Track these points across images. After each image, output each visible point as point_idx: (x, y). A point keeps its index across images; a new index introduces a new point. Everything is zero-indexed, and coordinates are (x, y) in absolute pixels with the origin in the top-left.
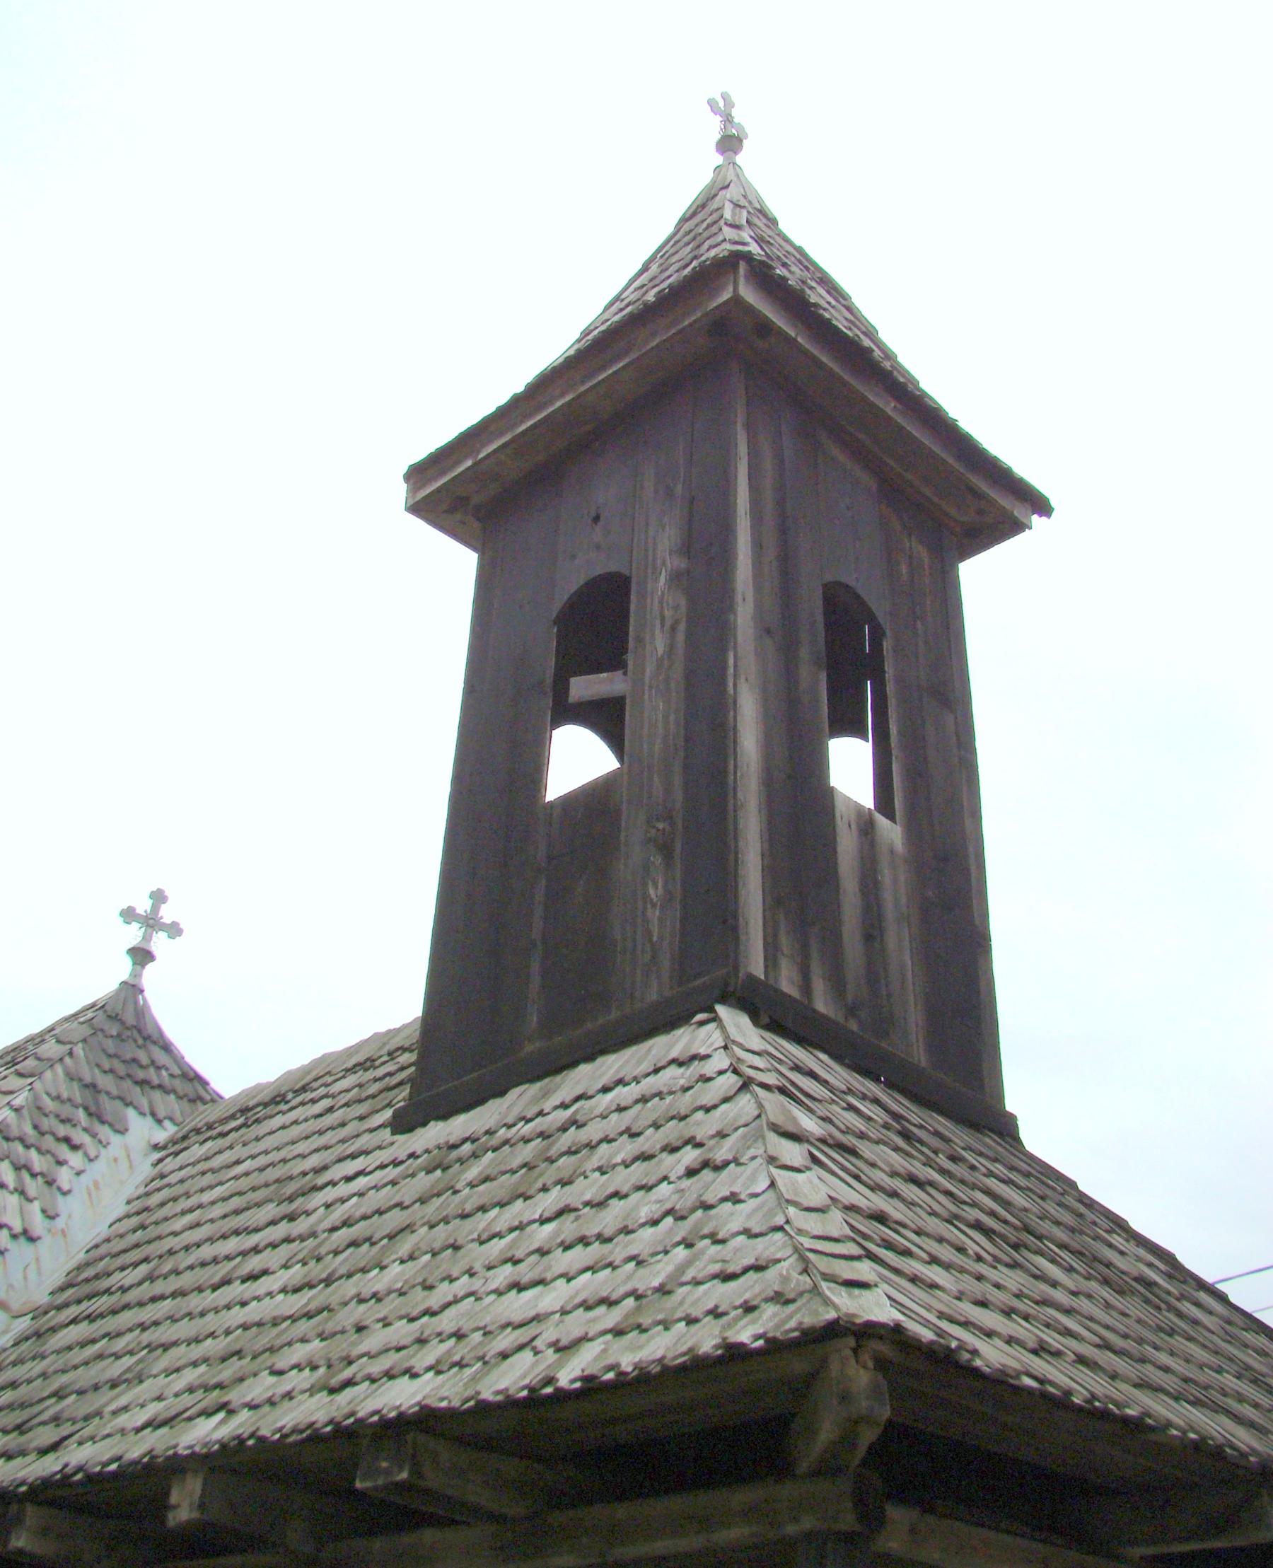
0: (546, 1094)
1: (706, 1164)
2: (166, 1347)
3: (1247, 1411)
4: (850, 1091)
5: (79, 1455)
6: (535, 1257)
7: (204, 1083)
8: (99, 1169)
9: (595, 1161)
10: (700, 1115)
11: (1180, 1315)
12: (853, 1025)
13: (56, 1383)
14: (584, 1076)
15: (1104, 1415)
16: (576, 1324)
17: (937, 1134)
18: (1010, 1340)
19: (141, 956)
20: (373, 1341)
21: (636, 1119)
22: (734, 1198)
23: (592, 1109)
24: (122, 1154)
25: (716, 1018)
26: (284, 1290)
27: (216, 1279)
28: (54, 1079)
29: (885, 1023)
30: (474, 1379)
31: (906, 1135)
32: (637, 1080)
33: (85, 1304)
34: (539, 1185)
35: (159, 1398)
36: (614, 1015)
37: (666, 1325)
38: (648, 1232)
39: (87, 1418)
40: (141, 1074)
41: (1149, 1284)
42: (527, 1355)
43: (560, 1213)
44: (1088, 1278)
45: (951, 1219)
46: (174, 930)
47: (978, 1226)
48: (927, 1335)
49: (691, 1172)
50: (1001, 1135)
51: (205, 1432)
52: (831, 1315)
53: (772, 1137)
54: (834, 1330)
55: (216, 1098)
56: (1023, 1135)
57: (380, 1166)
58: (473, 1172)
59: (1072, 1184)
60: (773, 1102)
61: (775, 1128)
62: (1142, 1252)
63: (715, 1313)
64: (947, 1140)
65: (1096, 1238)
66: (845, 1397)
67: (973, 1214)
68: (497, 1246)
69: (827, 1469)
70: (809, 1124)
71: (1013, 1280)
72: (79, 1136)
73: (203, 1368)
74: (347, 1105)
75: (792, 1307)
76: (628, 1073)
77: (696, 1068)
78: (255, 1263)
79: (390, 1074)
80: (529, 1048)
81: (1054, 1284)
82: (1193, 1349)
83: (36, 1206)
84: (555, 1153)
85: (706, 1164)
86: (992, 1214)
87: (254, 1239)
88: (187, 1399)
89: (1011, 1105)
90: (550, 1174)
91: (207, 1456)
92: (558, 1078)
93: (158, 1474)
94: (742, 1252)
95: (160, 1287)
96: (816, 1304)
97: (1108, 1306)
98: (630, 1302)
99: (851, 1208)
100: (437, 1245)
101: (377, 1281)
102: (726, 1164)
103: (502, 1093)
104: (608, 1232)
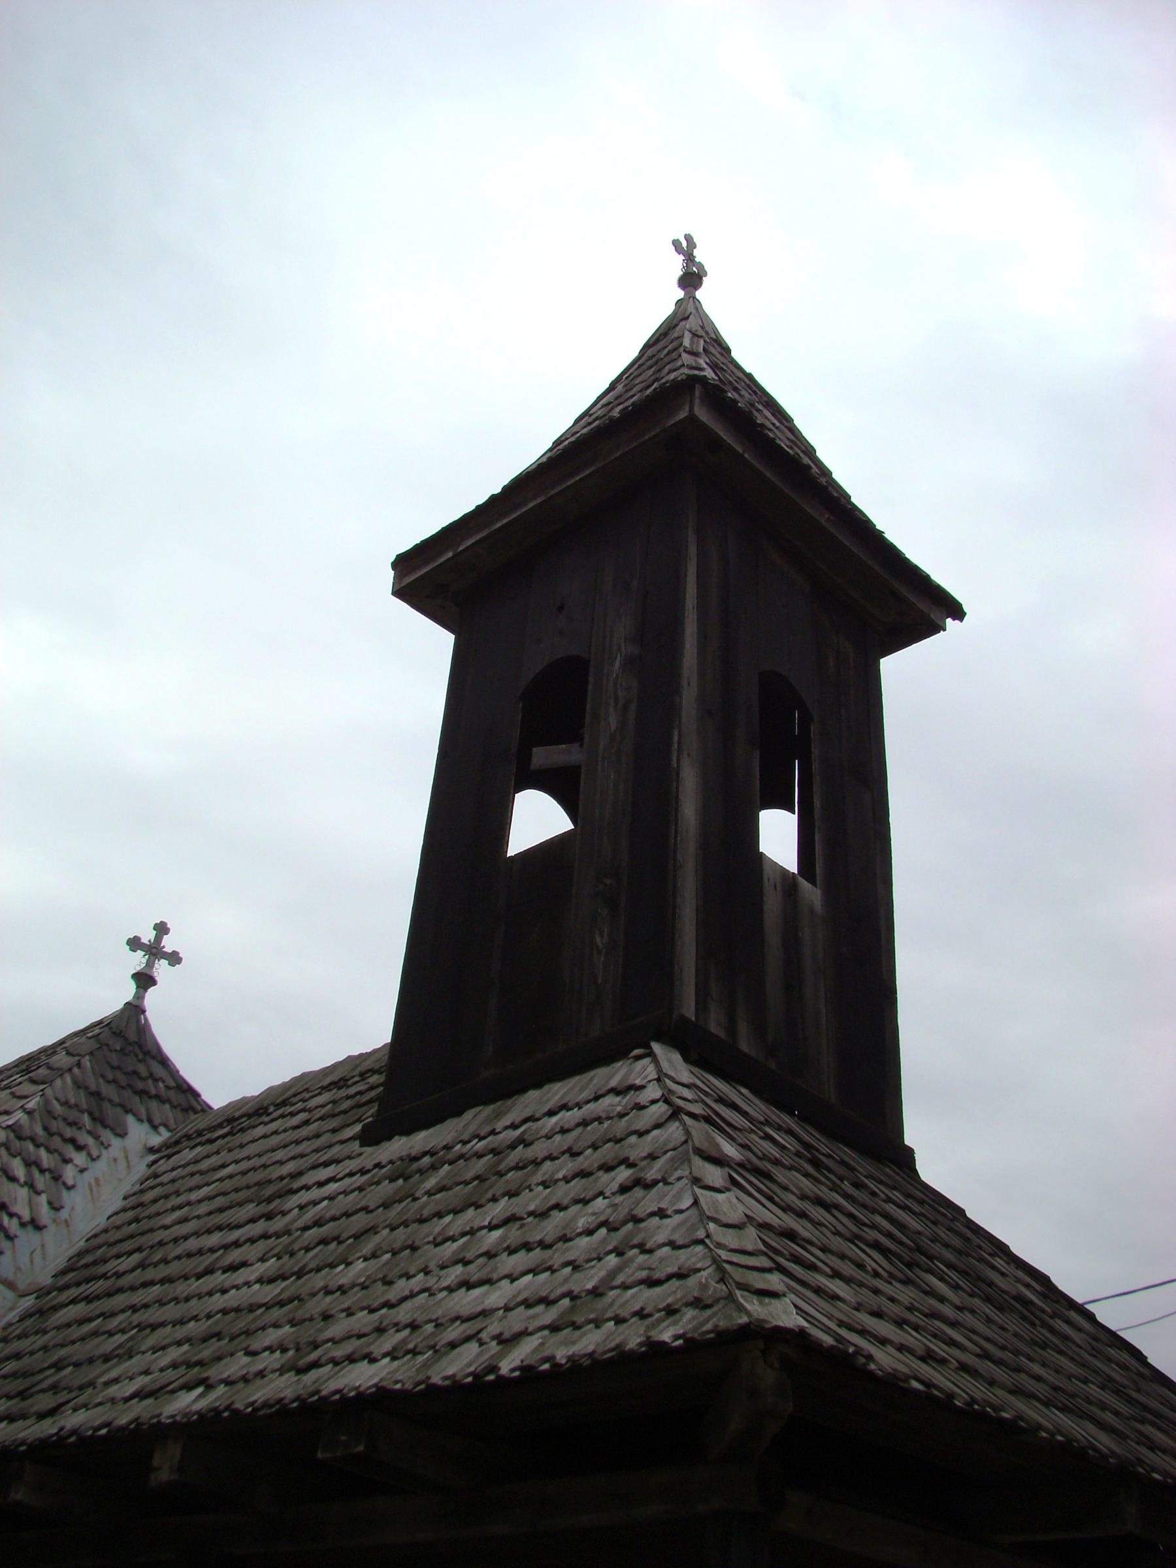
0: (498, 1115)
2: (154, 1327)
4: (767, 1123)
5: (73, 1420)
8: (100, 1168)
10: (633, 1139)
11: (1052, 1330)
12: (772, 1065)
14: (531, 1101)
16: (517, 1320)
17: (842, 1162)
18: (901, 1348)
21: (576, 1140)
22: (661, 1214)
23: (538, 1130)
24: (120, 1155)
25: (651, 1054)
26: (260, 1281)
27: (201, 1268)
28: (63, 1086)
30: (426, 1365)
32: (579, 1106)
34: (489, 1195)
38: (584, 1241)
40: (140, 1085)
41: (1026, 1303)
42: (473, 1347)
45: (853, 1239)
46: (174, 959)
47: (876, 1245)
48: (828, 1340)
50: (900, 1167)
52: (745, 1319)
53: (697, 1161)
55: (206, 1108)
58: (431, 1182)
59: (962, 1212)
62: (1020, 1274)
63: (641, 1314)
64: (852, 1169)
65: (981, 1260)
67: (873, 1235)
68: (450, 1248)
70: (730, 1150)
71: (906, 1294)
72: (84, 1138)
73: (186, 1347)
74: (322, 1118)
75: (709, 1312)
76: (572, 1099)
77: (631, 1098)
78: (235, 1256)
79: (361, 1093)
83: (43, 1198)
86: (889, 1235)
88: (170, 1374)
90: (500, 1186)
92: (509, 1102)
94: (667, 1261)
95: (150, 1274)
98: (566, 1302)
99: (764, 1226)
101: (344, 1275)
102: (655, 1183)
103: (459, 1113)
104: (549, 1239)
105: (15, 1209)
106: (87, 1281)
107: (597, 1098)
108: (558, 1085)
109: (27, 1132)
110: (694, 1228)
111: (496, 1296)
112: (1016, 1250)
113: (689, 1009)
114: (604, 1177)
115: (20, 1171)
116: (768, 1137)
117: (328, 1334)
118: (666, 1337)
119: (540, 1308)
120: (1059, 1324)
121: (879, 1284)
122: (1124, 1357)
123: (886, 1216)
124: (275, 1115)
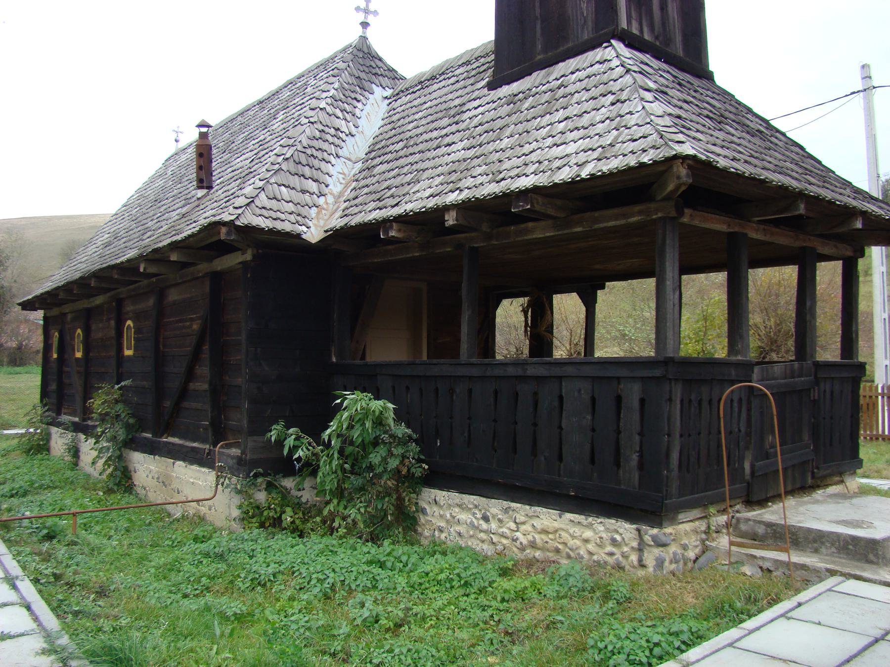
0: (548, 75)
1: (618, 101)
2: (424, 171)
3: (794, 174)
4: (660, 69)
5: (409, 207)
6: (560, 135)
7: (396, 72)
8: (368, 108)
9: (574, 100)
10: (612, 82)
11: (771, 142)
12: (658, 43)
13: (386, 184)
14: (561, 68)
15: (754, 179)
16: (582, 157)
17: (688, 82)
18: (725, 157)
19: (365, 25)
20: (507, 165)
21: (587, 84)
22: (631, 113)
23: (569, 81)
24: (374, 102)
25: (611, 45)
26: (464, 149)
27: (434, 146)
28: (345, 76)
29: (668, 41)
30: (550, 176)
31: (680, 84)
32: (584, 69)
33: (382, 157)
34: (555, 109)
35: (430, 187)
36: (570, 45)
37: (616, 157)
38: (600, 125)
39: (404, 195)
40: (374, 71)
41: (761, 132)
42: (567, 168)
43: (566, 119)
44: (742, 132)
45: (699, 115)
46: (375, 13)
47: (708, 117)
48: (704, 158)
49: (613, 104)
50: (708, 79)
51: (452, 198)
52: (674, 153)
53: (641, 91)
54: (676, 157)
55: (403, 78)
56: (716, 79)
57: (486, 105)
58: (527, 105)
59: (733, 96)
60: (638, 77)
61: (641, 87)
62: (757, 120)
63: (632, 152)
64: (692, 84)
65: (743, 116)
66: (678, 177)
67: (706, 112)
68: (543, 132)
69: (667, 198)
70: (652, 85)
71: (721, 135)
72: (360, 97)
73: (442, 177)
74: (464, 79)
75: (659, 150)
76: (580, 66)
77: (606, 66)
78: (447, 140)
79: (479, 67)
80: (539, 57)
81: (733, 135)
82: (777, 155)
83: (351, 124)
84: (556, 99)
85: (618, 101)
86: (711, 111)
87: (444, 132)
88: (441, 188)
89: (711, 69)
90: (558, 105)
91: (458, 204)
92: (551, 68)
93: (440, 212)
94: (639, 132)
95: (411, 150)
96: (667, 149)
97: (750, 141)
98: (600, 149)
99: (670, 115)
100: (520, 131)
101: (498, 145)
102: (625, 101)
103: (530, 74)
104: (586, 126)
105: (342, 130)
106: (383, 155)
107: (592, 66)
108: (572, 60)
109: (338, 98)
110: (644, 118)
111: (571, 148)
112: (755, 110)
113: (624, 25)
114: (604, 99)
115: (340, 114)
116: (661, 76)
117: (504, 167)
118: (645, 160)
119: (590, 152)
120: (773, 139)
121: (711, 132)
122: (797, 149)
123: (708, 103)
124: (441, 79)
